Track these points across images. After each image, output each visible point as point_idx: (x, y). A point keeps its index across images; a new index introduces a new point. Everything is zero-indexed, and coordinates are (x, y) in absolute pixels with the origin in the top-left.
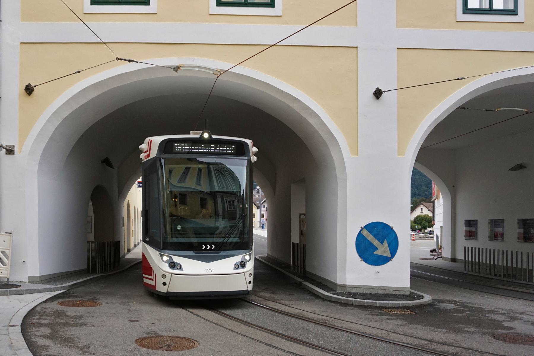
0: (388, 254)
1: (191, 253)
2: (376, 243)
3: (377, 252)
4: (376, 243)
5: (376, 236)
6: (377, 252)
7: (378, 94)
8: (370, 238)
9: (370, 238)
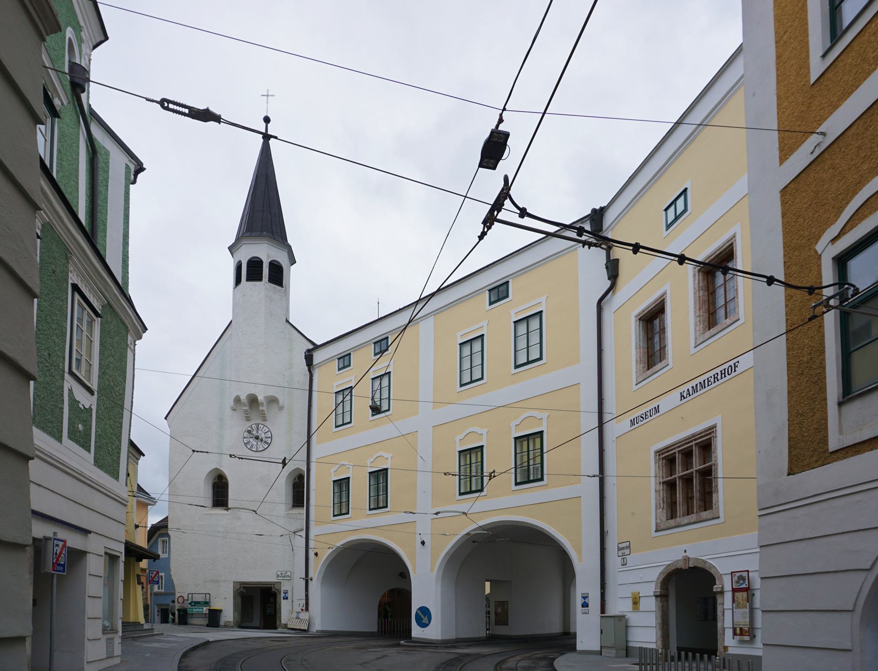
8: (420, 614)
9: (420, 614)
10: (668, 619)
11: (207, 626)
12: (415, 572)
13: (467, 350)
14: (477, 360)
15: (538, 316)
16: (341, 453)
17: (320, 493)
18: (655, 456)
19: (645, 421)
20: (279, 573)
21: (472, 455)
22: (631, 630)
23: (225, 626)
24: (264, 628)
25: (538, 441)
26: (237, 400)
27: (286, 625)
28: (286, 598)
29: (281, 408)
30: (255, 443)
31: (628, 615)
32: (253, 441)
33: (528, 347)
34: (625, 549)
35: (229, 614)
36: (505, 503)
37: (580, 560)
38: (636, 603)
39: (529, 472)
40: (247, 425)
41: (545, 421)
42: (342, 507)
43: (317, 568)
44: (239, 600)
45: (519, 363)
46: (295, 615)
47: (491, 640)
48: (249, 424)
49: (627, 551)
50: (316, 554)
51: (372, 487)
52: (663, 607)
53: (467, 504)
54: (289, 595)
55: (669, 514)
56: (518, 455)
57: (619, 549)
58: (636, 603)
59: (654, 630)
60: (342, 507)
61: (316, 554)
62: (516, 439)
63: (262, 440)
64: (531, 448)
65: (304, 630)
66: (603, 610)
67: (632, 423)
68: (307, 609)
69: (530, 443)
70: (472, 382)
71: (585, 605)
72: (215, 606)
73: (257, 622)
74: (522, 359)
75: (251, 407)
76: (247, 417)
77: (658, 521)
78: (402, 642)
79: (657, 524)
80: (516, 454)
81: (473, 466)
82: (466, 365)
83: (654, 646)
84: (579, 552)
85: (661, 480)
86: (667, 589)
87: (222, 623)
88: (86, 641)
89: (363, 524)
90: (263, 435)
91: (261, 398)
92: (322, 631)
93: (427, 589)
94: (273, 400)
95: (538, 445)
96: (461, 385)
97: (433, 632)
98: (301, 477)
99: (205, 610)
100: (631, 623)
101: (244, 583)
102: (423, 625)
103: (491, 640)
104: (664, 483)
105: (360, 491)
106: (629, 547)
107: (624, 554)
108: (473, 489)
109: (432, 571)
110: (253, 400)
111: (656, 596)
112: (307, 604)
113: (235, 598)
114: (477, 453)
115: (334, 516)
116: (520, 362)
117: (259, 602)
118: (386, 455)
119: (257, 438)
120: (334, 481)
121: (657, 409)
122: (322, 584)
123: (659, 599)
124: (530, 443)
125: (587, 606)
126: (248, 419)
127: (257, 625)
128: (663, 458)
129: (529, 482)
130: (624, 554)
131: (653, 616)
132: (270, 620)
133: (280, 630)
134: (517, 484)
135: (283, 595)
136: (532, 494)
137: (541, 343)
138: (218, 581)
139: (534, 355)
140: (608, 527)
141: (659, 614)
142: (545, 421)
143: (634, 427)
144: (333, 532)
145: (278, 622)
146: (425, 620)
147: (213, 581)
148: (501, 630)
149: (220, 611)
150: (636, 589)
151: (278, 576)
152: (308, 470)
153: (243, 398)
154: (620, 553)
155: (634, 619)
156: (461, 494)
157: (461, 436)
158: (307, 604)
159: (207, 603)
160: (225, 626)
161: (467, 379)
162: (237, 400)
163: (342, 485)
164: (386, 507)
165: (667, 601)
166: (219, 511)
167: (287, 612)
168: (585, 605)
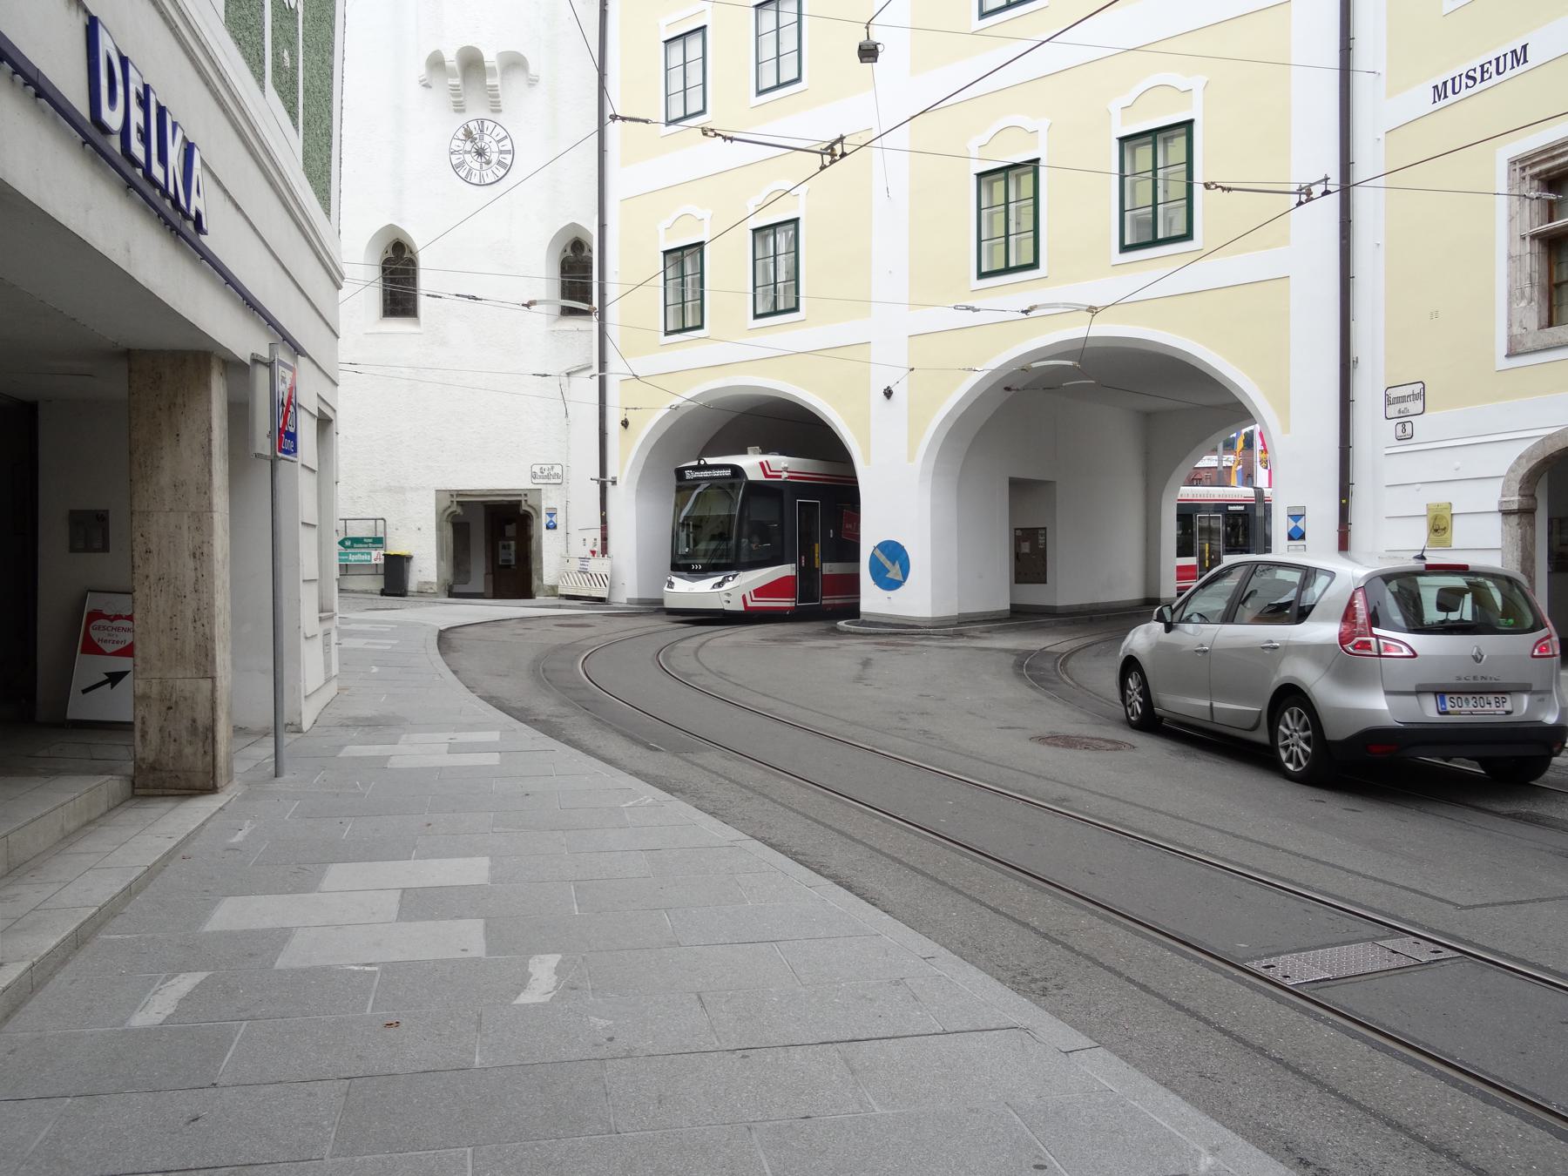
2: (888, 564)
3: (889, 575)
4: (888, 564)
5: (888, 557)
6: (889, 575)
7: (888, 393)
8: (883, 558)
9: (883, 558)
11: (383, 593)
16: (669, 191)
17: (632, 276)
18: (1511, 171)
19: (1479, 86)
20: (536, 469)
21: (1010, 183)
23: (421, 593)
24: (495, 597)
25: (1027, 180)
26: (436, 63)
27: (554, 588)
28: (552, 527)
29: (533, 82)
30: (476, 165)
32: (473, 162)
34: (1406, 403)
35: (427, 567)
36: (1092, 292)
37: (1286, 428)
40: (461, 120)
41: (1198, 96)
42: (686, 303)
43: (626, 458)
44: (449, 532)
46: (575, 565)
47: (1020, 616)
48: (461, 120)
49: (1416, 406)
50: (625, 424)
52: (1523, 538)
53: (690, 351)
54: (559, 519)
55: (1545, 314)
56: (984, 213)
57: (1389, 401)
60: (686, 303)
61: (625, 424)
63: (488, 162)
64: (1012, 198)
65: (601, 600)
67: (1439, 92)
68: (604, 550)
69: (1158, 152)
70: (779, 86)
72: (396, 547)
73: (478, 581)
74: (677, 112)
75: (464, 81)
76: (457, 104)
77: (1516, 330)
78: (841, 623)
79: (1511, 338)
80: (754, 260)
82: (768, 51)
84: (1283, 407)
85: (1528, 231)
86: (1533, 496)
87: (412, 586)
89: (742, 356)
90: (494, 147)
91: (490, 58)
92: (641, 601)
93: (901, 497)
94: (514, 63)
95: (1027, 190)
97: (915, 599)
99: (376, 557)
101: (459, 493)
102: (887, 583)
103: (1020, 616)
104: (1533, 237)
105: (729, 274)
106: (1421, 396)
107: (1403, 414)
108: (689, 324)
109: (911, 458)
110: (472, 63)
111: (1506, 513)
112: (604, 538)
113: (439, 528)
114: (1018, 177)
116: (764, 85)
117: (495, 539)
118: (1027, 122)
119: (480, 153)
120: (666, 253)
121: (1520, 56)
122: (934, 474)
123: (1514, 520)
124: (1158, 152)
125: (1303, 537)
126: (459, 108)
127: (481, 589)
128: (1533, 177)
130: (1403, 414)
132: (514, 577)
133: (540, 599)
134: (1124, 248)
135: (545, 519)
136: (782, 334)
137: (799, 50)
138: (401, 490)
139: (789, 73)
140: (1358, 349)
142: (1198, 96)
143: (1443, 102)
144: (674, 374)
145: (535, 582)
146: (894, 572)
147: (389, 489)
148: (1033, 595)
149: (408, 558)
150: (1439, 496)
151: (534, 476)
153: (451, 57)
154: (1393, 410)
156: (981, 275)
157: (668, 223)
158: (604, 538)
159: (378, 541)
160: (421, 593)
161: (769, 80)
162: (436, 63)
163: (685, 260)
164: (701, 327)
165: (1533, 525)
166: (398, 325)
167: (558, 556)
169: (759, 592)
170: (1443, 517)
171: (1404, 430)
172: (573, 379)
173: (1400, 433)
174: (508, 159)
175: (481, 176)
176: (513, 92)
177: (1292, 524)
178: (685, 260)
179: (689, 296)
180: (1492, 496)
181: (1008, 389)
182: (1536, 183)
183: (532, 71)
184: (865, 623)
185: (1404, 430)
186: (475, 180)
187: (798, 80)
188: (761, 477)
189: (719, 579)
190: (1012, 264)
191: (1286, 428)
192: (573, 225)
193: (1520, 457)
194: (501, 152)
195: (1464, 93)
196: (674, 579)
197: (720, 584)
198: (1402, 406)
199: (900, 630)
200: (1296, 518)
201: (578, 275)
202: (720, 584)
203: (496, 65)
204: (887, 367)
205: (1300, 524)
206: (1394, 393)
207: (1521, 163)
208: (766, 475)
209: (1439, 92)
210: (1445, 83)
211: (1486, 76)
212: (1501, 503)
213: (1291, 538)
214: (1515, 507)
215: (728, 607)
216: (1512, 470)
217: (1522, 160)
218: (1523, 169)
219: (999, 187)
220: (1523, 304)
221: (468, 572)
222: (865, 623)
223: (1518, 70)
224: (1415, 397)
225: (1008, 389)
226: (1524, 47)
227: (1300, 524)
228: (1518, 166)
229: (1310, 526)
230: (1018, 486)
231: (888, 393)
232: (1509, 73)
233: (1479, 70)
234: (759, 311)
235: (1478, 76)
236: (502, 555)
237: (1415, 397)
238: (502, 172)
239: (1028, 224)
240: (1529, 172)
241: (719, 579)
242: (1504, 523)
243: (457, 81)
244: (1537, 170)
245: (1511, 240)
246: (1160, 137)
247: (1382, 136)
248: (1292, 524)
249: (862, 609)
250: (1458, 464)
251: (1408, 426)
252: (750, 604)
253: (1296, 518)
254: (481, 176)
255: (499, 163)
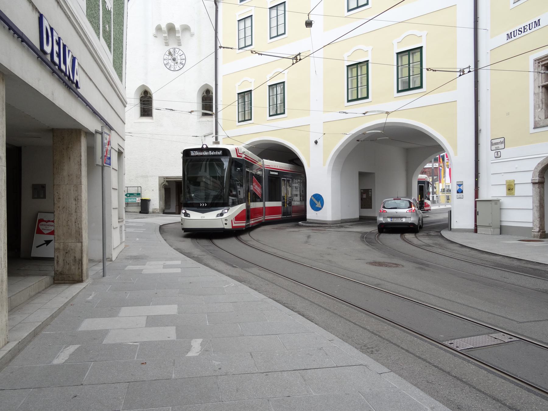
0: (320, 207)
1: (196, 209)
2: (316, 202)
4: (316, 202)
7: (316, 142)
8: (314, 200)
9: (314, 200)
10: (544, 202)
11: (140, 212)
12: (309, 166)
13: (274, 12)
14: (281, 21)
15: (250, 18)
18: (535, 63)
19: (523, 34)
21: (358, 69)
22: (504, 212)
23: (153, 212)
25: (364, 68)
29: (192, 35)
30: (173, 64)
31: (503, 200)
32: (171, 63)
33: (245, 37)
34: (498, 145)
35: (156, 203)
36: (387, 107)
37: (456, 154)
38: (510, 188)
39: (278, 109)
40: (167, 48)
42: (245, 112)
45: (351, 8)
48: (167, 48)
49: (501, 146)
51: (240, 104)
52: (540, 192)
57: (492, 144)
58: (510, 188)
59: (531, 212)
60: (245, 112)
62: (398, 54)
64: (359, 74)
66: (476, 196)
67: (509, 36)
70: (278, 36)
71: (460, 191)
74: (242, 45)
75: (168, 35)
77: (537, 119)
78: (300, 223)
79: (535, 122)
81: (278, 96)
83: (531, 225)
84: (455, 147)
85: (541, 84)
86: (543, 177)
87: (150, 210)
88: (113, 229)
90: (179, 58)
91: (177, 27)
93: (322, 178)
94: (186, 28)
95: (364, 71)
96: (271, 38)
97: (327, 214)
98: (208, 92)
99: (138, 200)
100: (504, 207)
101: (167, 178)
102: (316, 209)
103: (363, 220)
104: (543, 86)
105: (260, 101)
106: (504, 142)
107: (497, 149)
108: (247, 118)
109: (324, 165)
110: (171, 29)
111: (534, 183)
113: (160, 190)
114: (361, 67)
115: (270, 116)
119: (174, 60)
120: (238, 94)
121: (537, 23)
123: (537, 186)
125: (462, 192)
126: (167, 44)
127: (174, 211)
128: (542, 66)
129: (410, 89)
130: (497, 149)
131: (530, 200)
134: (399, 91)
136: (279, 122)
138: (147, 177)
139: (281, 31)
141: (538, 198)
143: (510, 40)
146: (318, 205)
149: (149, 200)
150: (510, 177)
152: (216, 85)
153: (164, 27)
154: (494, 147)
155: (507, 202)
159: (139, 195)
160: (153, 212)
161: (274, 34)
163: (245, 96)
166: (146, 120)
168: (460, 191)
169: (238, 218)
170: (511, 185)
171: (498, 154)
172: (206, 138)
173: (496, 156)
174: (183, 57)
175: (174, 68)
176: (185, 39)
177: (458, 187)
178: (245, 96)
179: (247, 109)
180: (529, 177)
181: (358, 141)
182: (543, 67)
183: (192, 30)
184: (308, 223)
185: (498, 154)
186: (172, 69)
187: (284, 34)
188: (236, 157)
189: (220, 212)
190: (359, 97)
191: (456, 154)
192: (206, 84)
193: (539, 164)
194: (181, 59)
195: (518, 36)
196: (188, 212)
197: (222, 214)
198: (497, 146)
199: (321, 225)
200: (460, 185)
201: (208, 101)
202: (222, 214)
203: (180, 29)
204: (316, 133)
205: (461, 187)
206: (494, 141)
207: (538, 61)
208: (238, 156)
209: (509, 36)
210: (511, 33)
211: (525, 30)
212: (532, 180)
213: (458, 192)
214: (537, 181)
215: (226, 227)
216: (536, 168)
217: (538, 60)
218: (539, 63)
219: (355, 70)
220: (539, 110)
221: (170, 205)
222: (308, 223)
223: (537, 28)
224: (501, 143)
225: (358, 141)
226: (539, 20)
227: (461, 187)
228: (537, 62)
229: (465, 188)
230: (362, 175)
231: (316, 142)
232: (533, 29)
233: (523, 28)
234: (271, 114)
235: (523, 30)
236: (182, 199)
237: (501, 143)
238: (182, 66)
239: (365, 83)
240: (541, 64)
241: (220, 212)
242: (533, 187)
243: (166, 35)
244: (544, 63)
245: (535, 87)
246: (411, 52)
247: (489, 51)
248: (458, 187)
249: (307, 218)
250: (516, 166)
251: (499, 153)
252: (234, 225)
253: (460, 185)
254: (174, 68)
255: (181, 63)
